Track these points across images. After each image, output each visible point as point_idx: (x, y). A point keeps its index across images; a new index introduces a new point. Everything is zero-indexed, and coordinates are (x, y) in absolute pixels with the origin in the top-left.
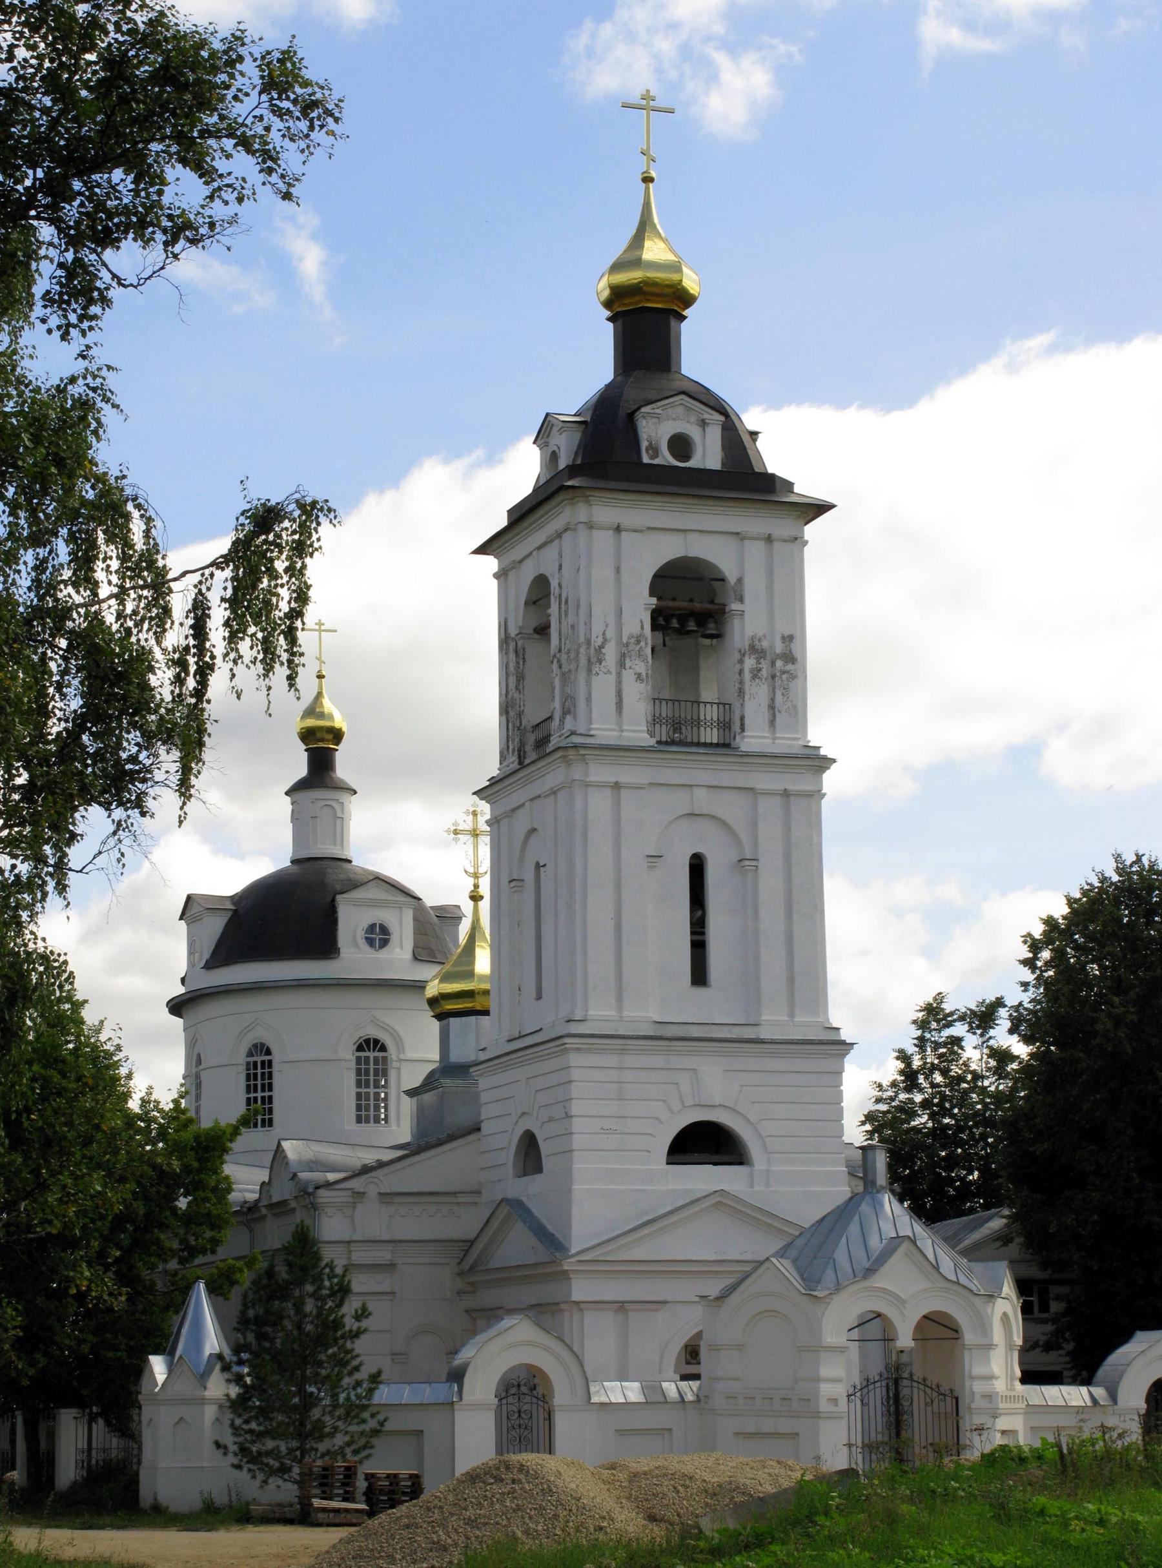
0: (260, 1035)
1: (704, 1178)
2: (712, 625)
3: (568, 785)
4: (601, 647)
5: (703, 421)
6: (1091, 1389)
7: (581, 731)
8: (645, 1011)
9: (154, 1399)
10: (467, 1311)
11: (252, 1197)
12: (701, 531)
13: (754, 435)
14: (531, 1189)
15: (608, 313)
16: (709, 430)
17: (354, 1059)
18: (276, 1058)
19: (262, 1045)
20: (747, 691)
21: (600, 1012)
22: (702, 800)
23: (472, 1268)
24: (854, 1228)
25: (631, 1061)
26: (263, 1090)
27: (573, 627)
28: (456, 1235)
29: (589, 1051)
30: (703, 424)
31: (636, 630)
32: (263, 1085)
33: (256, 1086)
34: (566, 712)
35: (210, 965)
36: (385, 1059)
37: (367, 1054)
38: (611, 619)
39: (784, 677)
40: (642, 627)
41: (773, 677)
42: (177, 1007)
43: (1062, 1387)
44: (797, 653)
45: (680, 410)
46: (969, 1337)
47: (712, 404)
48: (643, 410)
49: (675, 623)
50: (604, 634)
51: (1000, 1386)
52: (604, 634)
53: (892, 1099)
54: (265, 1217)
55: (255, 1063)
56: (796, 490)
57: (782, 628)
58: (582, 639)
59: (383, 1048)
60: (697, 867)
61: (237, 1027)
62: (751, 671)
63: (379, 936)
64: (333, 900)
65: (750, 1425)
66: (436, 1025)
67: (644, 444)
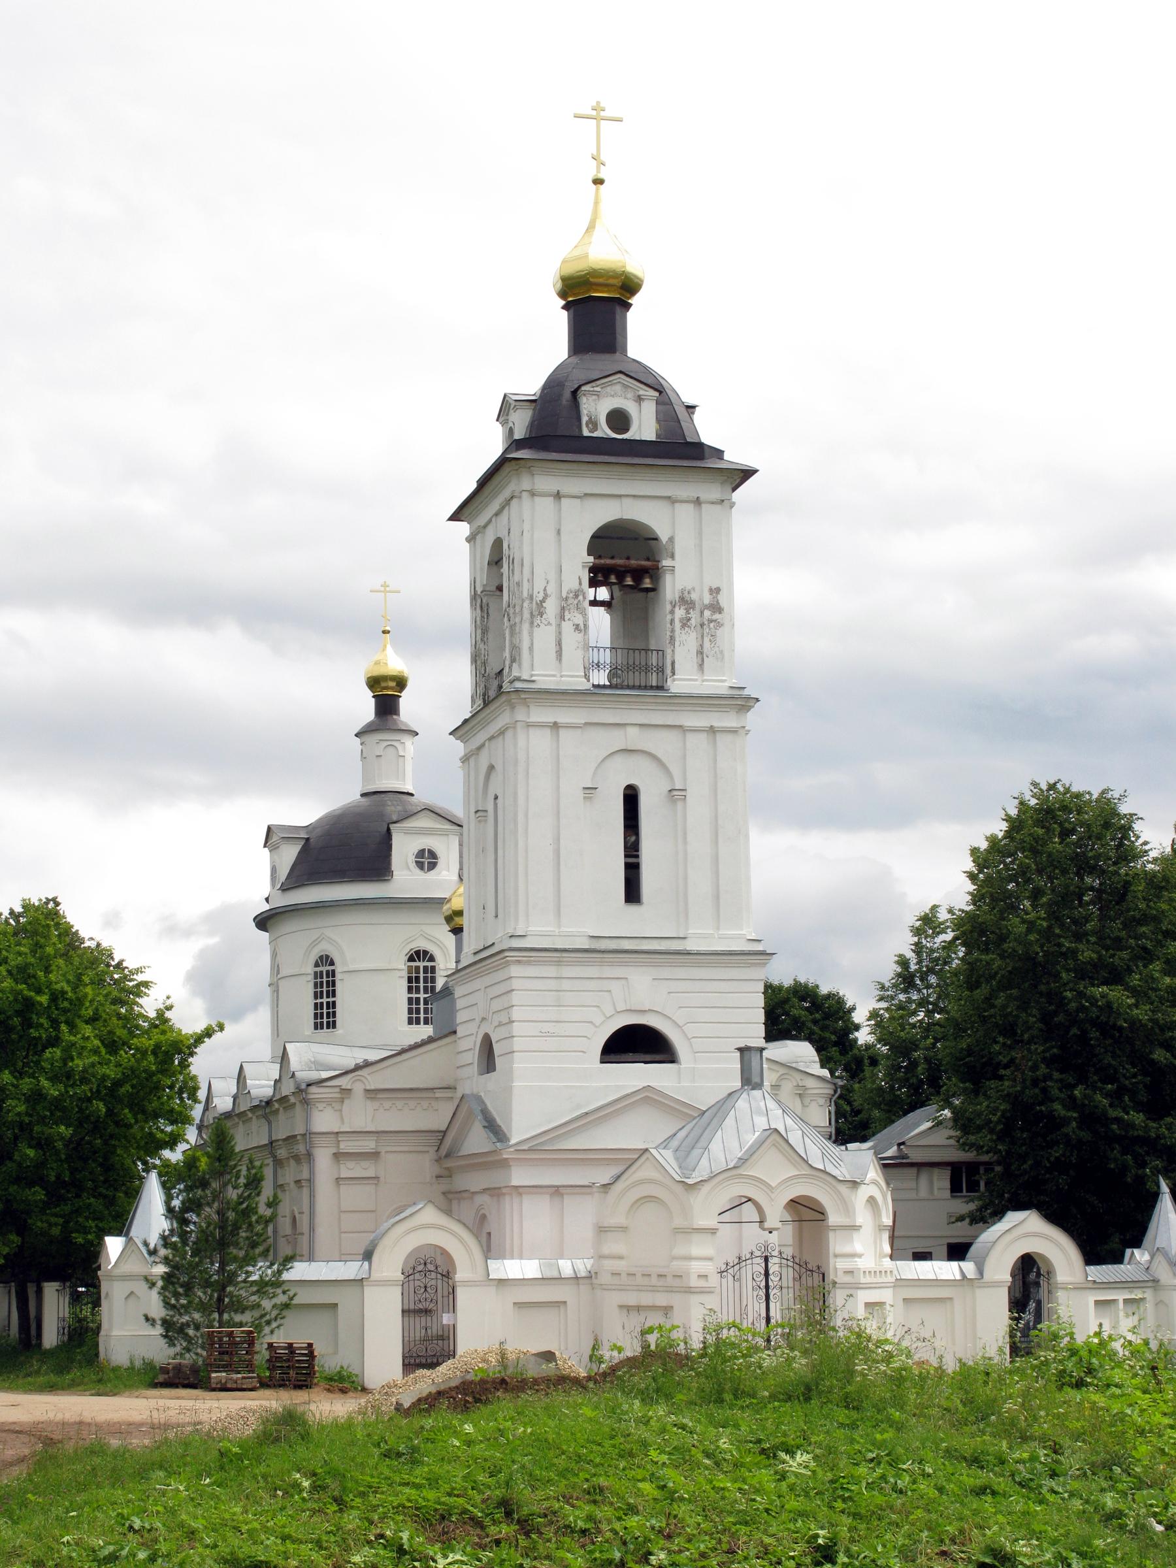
0: (325, 948)
1: (636, 1075)
2: (647, 580)
3: (513, 725)
4: (543, 601)
5: (639, 396)
6: (961, 1263)
7: (525, 677)
8: (577, 929)
9: (111, 1277)
10: (444, 1193)
11: (269, 1092)
12: (634, 496)
13: (691, 408)
14: (485, 1086)
15: (563, 303)
16: (645, 404)
17: (405, 968)
18: (339, 968)
19: (327, 957)
20: (677, 639)
21: (537, 926)
22: (633, 737)
23: (448, 1156)
24: (729, 1121)
25: (568, 971)
26: (328, 997)
27: (518, 584)
28: (435, 1127)
29: (529, 963)
30: (639, 399)
31: (575, 586)
32: (328, 992)
33: (322, 992)
34: (513, 660)
35: (285, 889)
36: (433, 969)
37: (417, 964)
38: (552, 577)
39: (712, 625)
40: (580, 584)
41: (702, 625)
42: (263, 922)
43: (934, 1262)
44: (723, 602)
45: (618, 388)
46: (833, 1219)
47: (649, 382)
48: (583, 388)
49: (629, 581)
50: (545, 590)
51: (866, 1263)
52: (545, 590)
53: (892, 998)
54: (278, 1110)
55: (321, 972)
56: (726, 457)
57: (710, 581)
58: (525, 594)
59: (432, 959)
60: (631, 799)
61: (302, 944)
62: (681, 620)
63: (427, 860)
64: (389, 830)
65: (632, 1299)
66: (452, 937)
67: (585, 419)
